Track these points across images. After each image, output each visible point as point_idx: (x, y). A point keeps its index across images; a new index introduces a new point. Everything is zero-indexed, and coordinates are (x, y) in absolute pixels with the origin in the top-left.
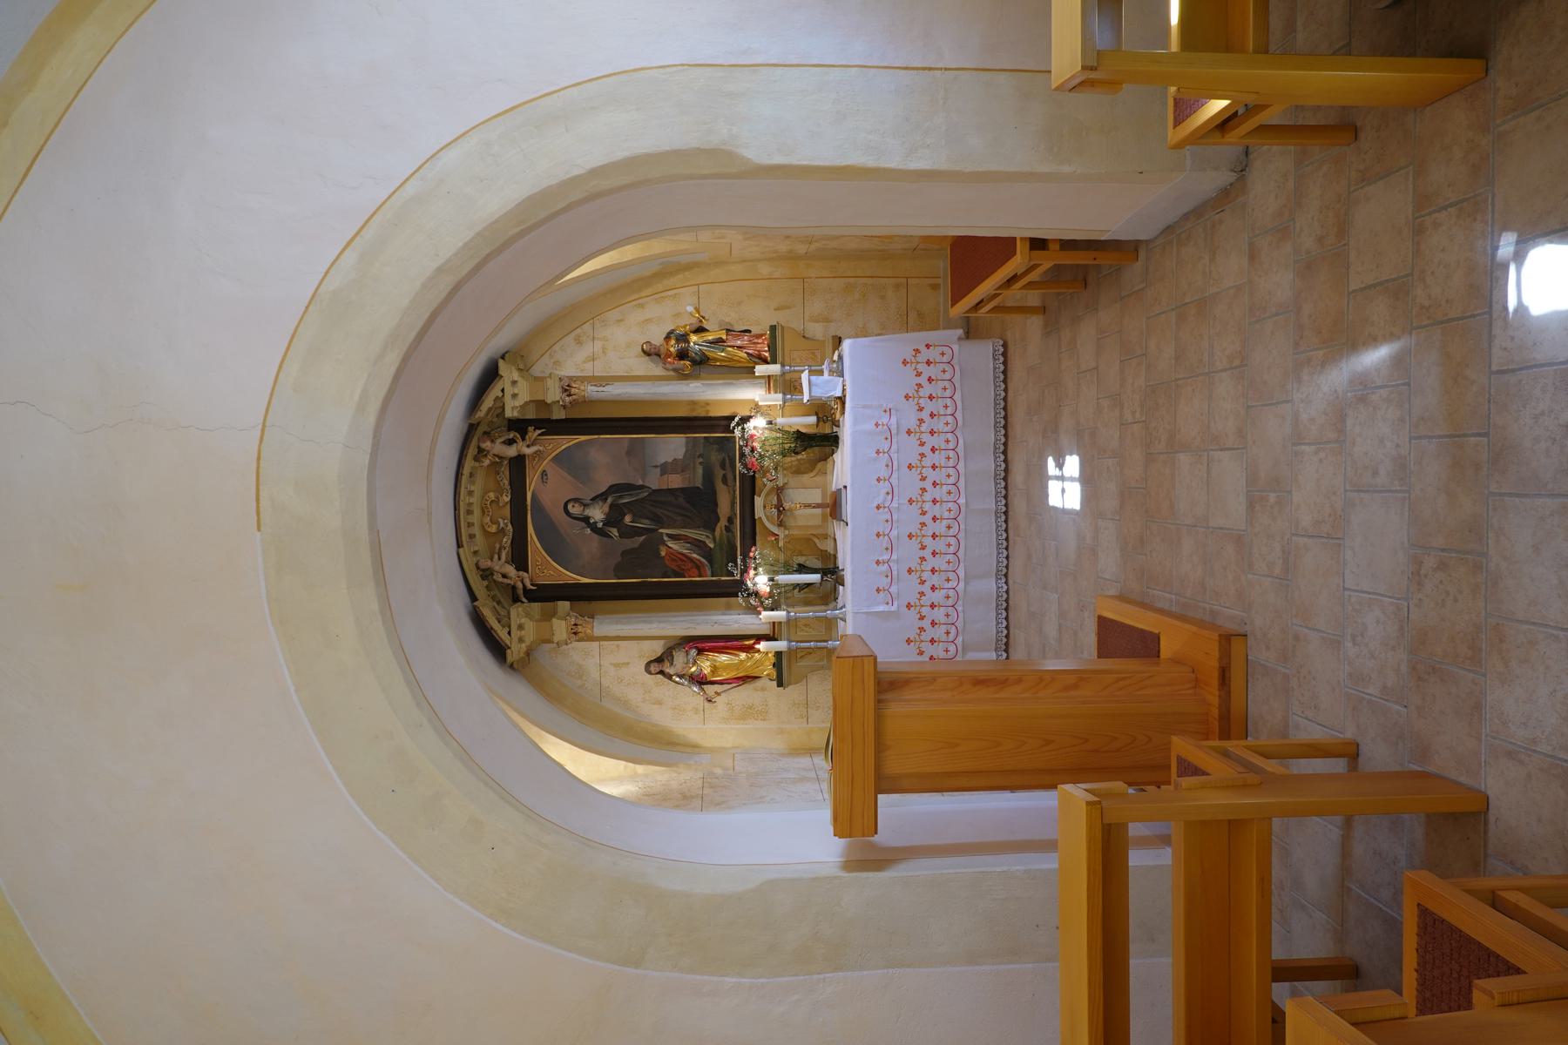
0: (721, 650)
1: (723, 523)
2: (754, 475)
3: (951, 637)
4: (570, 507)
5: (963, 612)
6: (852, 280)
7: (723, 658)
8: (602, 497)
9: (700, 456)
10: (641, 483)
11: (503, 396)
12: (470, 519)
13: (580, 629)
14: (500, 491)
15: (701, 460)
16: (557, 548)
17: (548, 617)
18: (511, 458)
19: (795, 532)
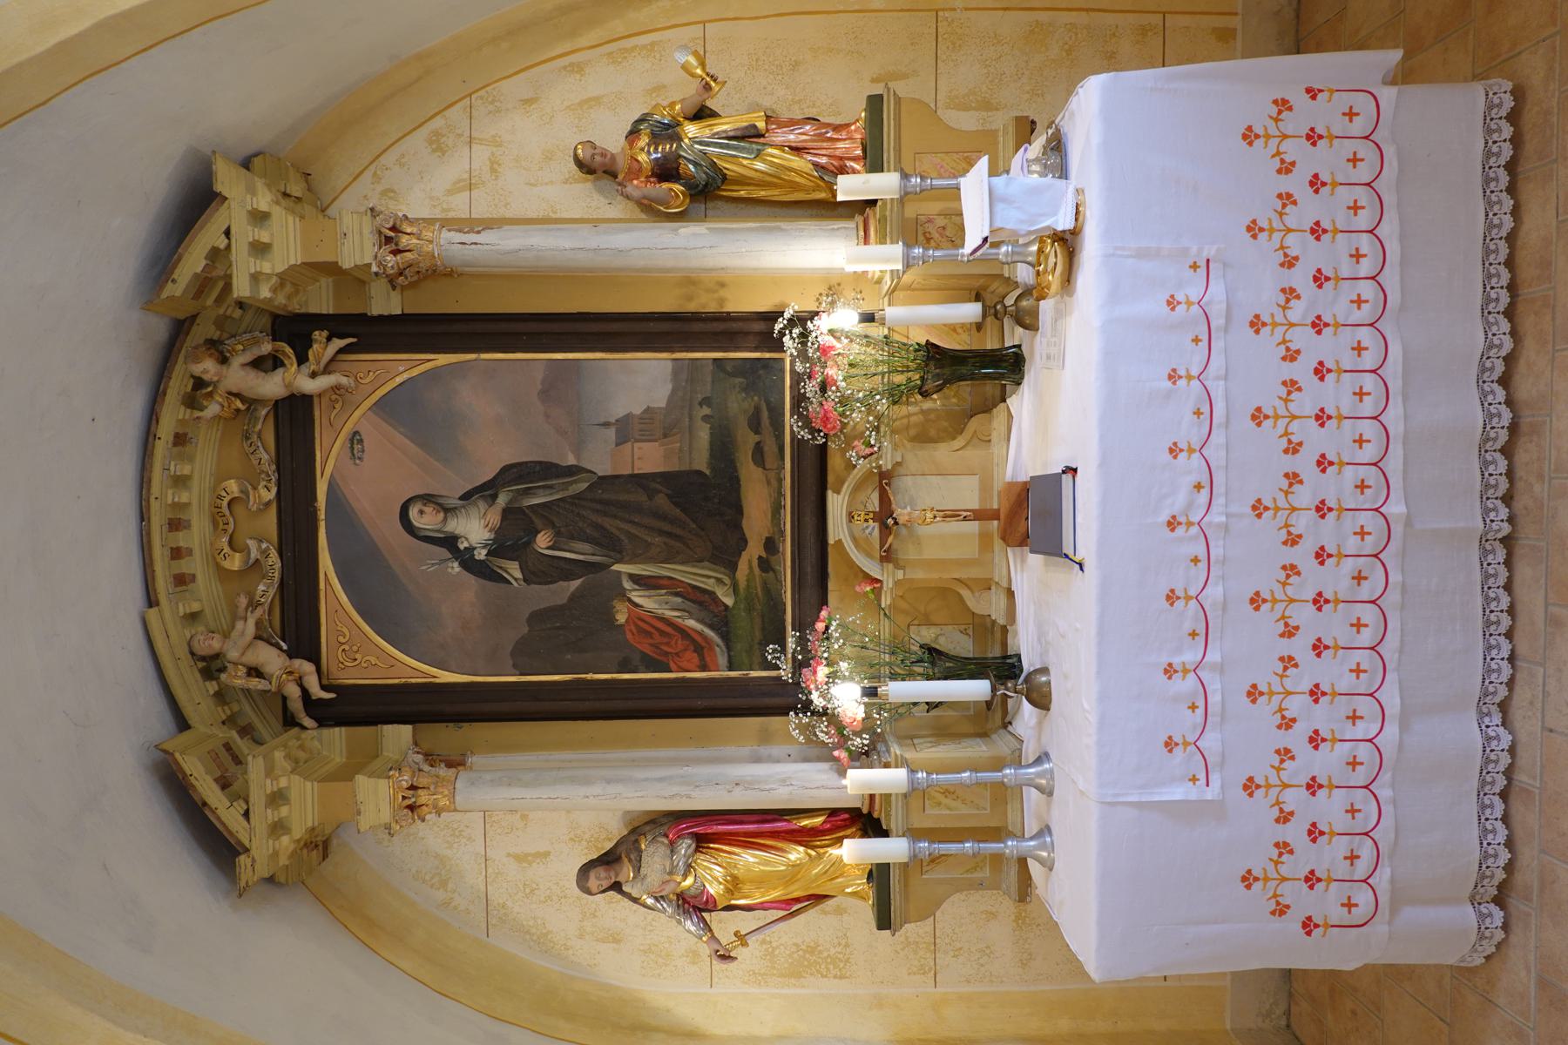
1: (754, 550)
2: (825, 443)
3: (1362, 868)
4: (413, 513)
5: (1394, 802)
6: (1044, 17)
7: (748, 859)
8: (485, 492)
9: (706, 401)
10: (571, 460)
11: (228, 247)
12: (181, 538)
13: (423, 797)
14: (251, 479)
15: (706, 411)
17: (361, 762)
18: (277, 401)
19: (919, 574)
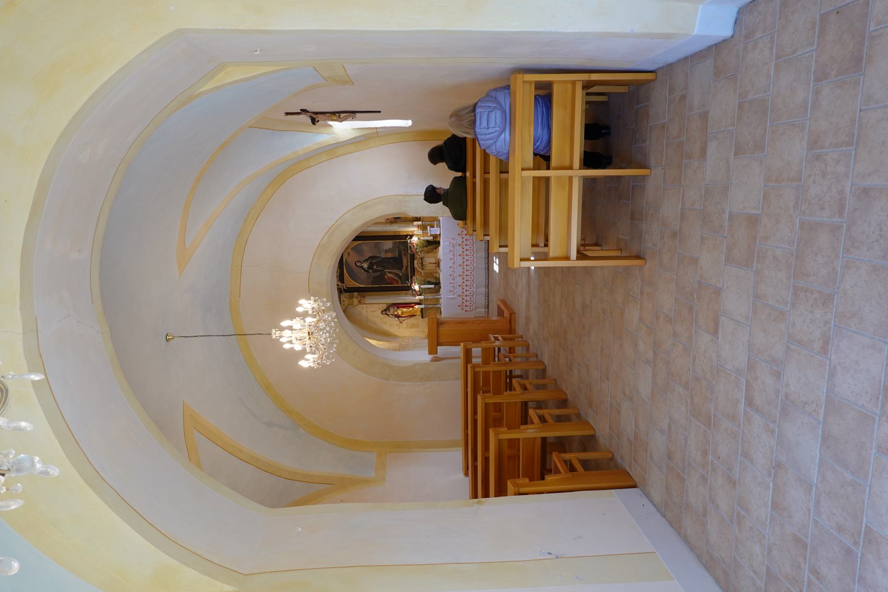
0: (404, 307)
1: (405, 268)
3: (472, 305)
4: (357, 263)
7: (405, 310)
8: (366, 260)
10: (378, 255)
13: (361, 301)
16: (353, 276)
17: (351, 297)
